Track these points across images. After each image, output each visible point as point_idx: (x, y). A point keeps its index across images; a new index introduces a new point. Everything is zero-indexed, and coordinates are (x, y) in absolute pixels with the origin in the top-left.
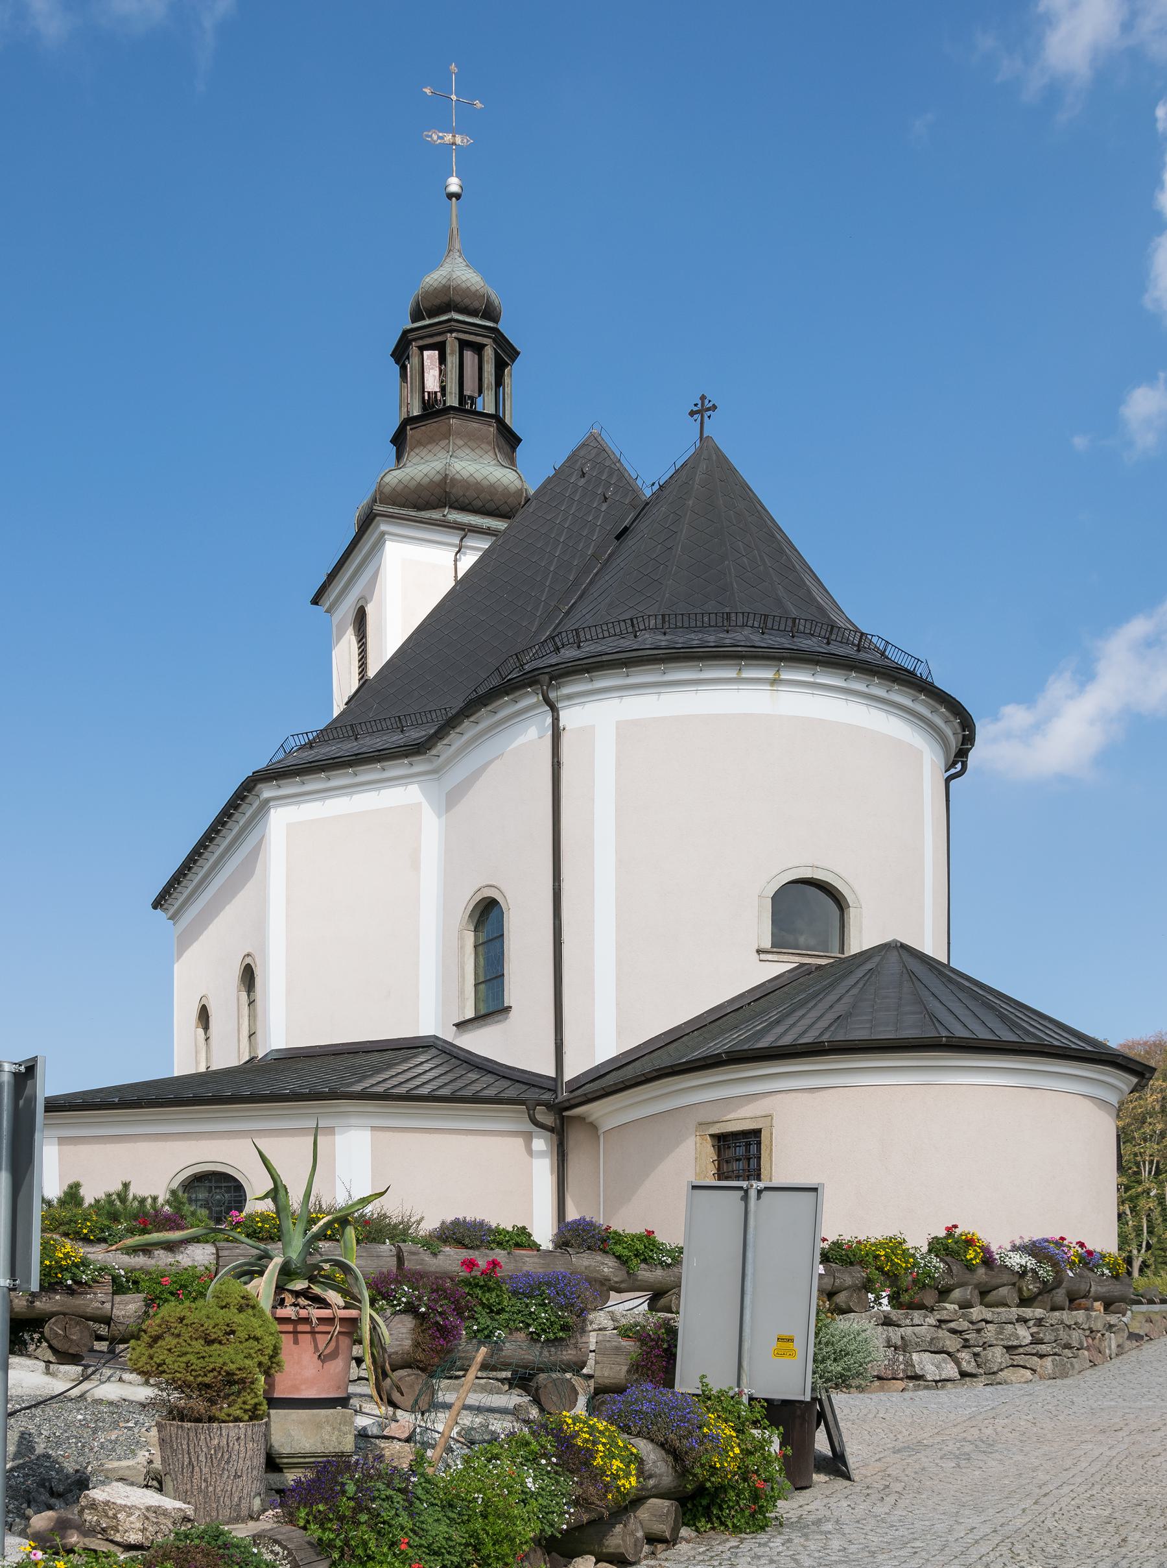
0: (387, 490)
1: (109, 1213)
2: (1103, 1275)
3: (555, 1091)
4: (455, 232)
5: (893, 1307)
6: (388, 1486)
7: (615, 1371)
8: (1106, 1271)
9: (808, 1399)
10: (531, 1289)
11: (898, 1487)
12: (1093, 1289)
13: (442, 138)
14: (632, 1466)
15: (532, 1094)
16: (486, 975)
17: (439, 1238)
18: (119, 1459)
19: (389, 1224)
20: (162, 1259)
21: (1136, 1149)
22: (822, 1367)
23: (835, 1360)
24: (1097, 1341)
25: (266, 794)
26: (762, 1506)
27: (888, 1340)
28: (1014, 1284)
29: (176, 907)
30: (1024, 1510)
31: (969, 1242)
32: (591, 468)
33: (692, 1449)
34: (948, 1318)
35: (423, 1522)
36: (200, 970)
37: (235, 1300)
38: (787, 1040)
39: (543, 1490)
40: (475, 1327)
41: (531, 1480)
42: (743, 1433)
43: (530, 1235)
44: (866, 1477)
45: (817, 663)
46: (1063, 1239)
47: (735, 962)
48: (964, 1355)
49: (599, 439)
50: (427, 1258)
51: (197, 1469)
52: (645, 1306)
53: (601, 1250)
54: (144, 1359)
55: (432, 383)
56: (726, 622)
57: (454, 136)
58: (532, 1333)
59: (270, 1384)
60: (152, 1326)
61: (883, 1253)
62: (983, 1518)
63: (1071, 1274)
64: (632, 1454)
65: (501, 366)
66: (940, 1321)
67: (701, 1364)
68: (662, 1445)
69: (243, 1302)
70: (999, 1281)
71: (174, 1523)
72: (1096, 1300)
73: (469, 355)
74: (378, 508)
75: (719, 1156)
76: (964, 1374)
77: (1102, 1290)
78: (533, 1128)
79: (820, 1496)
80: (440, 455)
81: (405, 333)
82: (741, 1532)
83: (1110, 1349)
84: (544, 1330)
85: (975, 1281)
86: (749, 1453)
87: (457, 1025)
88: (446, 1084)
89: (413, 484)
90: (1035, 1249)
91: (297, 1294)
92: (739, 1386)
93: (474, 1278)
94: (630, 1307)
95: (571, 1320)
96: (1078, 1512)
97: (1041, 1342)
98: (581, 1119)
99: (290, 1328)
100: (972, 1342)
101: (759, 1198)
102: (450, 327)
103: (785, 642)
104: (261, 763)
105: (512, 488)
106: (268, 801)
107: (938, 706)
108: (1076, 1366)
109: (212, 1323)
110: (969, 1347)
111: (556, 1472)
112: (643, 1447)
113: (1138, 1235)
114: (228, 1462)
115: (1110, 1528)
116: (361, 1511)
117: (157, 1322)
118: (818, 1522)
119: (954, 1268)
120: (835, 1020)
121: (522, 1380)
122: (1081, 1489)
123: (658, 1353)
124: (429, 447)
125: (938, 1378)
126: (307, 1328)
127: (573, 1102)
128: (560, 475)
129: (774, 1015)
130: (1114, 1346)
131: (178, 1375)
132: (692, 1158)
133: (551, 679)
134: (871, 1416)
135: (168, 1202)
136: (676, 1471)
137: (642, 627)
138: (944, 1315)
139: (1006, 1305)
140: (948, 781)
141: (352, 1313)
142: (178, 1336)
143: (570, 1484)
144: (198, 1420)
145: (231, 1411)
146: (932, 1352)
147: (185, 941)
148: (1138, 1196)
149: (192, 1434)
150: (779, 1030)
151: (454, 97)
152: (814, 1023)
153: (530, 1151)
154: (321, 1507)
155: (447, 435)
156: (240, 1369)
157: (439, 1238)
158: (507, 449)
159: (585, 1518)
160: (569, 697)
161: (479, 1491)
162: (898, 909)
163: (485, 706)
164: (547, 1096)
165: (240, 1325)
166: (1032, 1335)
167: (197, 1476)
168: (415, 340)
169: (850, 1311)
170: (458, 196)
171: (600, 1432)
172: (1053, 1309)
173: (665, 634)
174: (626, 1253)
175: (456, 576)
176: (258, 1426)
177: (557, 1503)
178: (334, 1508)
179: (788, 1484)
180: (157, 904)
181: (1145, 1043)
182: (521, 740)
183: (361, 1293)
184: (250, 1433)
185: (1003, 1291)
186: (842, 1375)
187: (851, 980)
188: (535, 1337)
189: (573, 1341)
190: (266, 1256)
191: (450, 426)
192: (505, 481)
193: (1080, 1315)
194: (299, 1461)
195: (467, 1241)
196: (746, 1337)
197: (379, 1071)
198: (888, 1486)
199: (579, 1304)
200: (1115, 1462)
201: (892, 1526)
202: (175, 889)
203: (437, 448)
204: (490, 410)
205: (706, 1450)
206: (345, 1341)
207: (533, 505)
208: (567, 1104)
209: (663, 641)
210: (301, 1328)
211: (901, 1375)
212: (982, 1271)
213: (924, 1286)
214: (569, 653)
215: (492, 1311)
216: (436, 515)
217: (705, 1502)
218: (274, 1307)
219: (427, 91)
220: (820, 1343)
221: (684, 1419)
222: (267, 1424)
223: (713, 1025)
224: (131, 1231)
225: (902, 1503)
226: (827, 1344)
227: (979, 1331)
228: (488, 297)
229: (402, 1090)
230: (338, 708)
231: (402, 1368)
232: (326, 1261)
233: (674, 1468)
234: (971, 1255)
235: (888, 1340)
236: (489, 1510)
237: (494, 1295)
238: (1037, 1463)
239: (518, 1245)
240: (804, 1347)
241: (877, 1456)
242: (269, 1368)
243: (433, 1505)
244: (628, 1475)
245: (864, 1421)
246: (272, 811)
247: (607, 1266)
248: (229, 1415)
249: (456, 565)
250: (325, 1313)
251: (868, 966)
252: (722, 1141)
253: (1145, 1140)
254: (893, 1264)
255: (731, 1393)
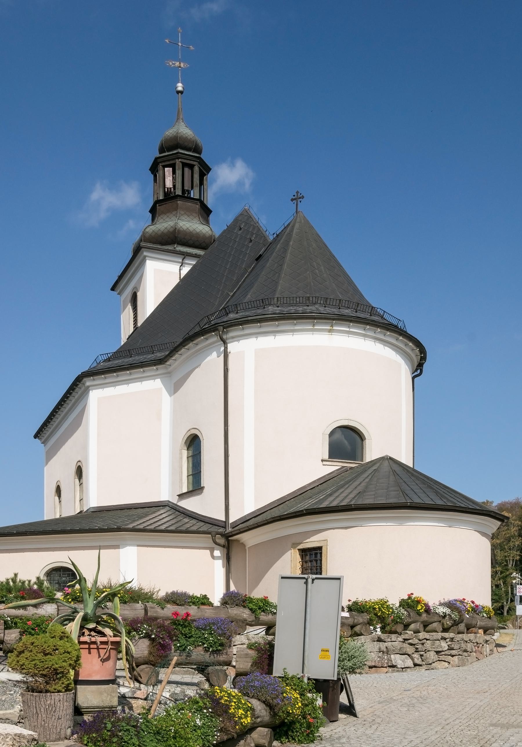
0: (147, 235)
1: (7, 588)
2: (483, 616)
3: (225, 527)
4: (180, 110)
5: (382, 632)
6: (128, 724)
7: (245, 665)
8: (485, 615)
9: (336, 679)
10: (208, 626)
11: (379, 720)
12: (478, 623)
13: (174, 64)
14: (249, 713)
15: (214, 529)
16: (192, 472)
17: (165, 600)
18: (6, 710)
19: (144, 593)
20: (31, 611)
21: (506, 554)
22: (342, 663)
23: (349, 660)
24: (480, 648)
25: (88, 384)
26: (312, 731)
27: (380, 649)
28: (440, 621)
29: (45, 437)
30: (436, 732)
31: (418, 602)
32: (244, 224)
33: (278, 704)
34: (408, 638)
35: (144, 742)
36: (58, 469)
37: (58, 634)
38: (334, 504)
39: (204, 724)
40: (178, 645)
41: (198, 720)
42: (304, 696)
43: (208, 599)
44: (364, 716)
45: (351, 321)
46: (464, 599)
47: (311, 466)
48: (416, 656)
49: (248, 211)
50: (159, 610)
51: (40, 715)
52: (264, 633)
53: (242, 606)
54: (14, 663)
55: (169, 183)
56: (308, 301)
57: (180, 63)
58: (205, 647)
59: (77, 674)
60: (20, 647)
61: (377, 607)
62: (417, 736)
63: (468, 616)
64: (249, 707)
65: (202, 176)
66: (404, 639)
67: (285, 663)
68: (264, 702)
69: (62, 635)
70: (433, 620)
71: (28, 742)
72: (480, 628)
73: (186, 170)
74: (143, 244)
75: (302, 559)
76: (416, 665)
77: (483, 624)
78: (214, 545)
79: (342, 725)
80: (172, 218)
81: (156, 159)
82: (302, 743)
83: (486, 652)
84: (211, 646)
85: (422, 620)
86: (307, 705)
87: (179, 496)
88: (173, 524)
89: (160, 232)
90: (450, 605)
91: (90, 630)
92: (303, 673)
93: (178, 621)
94: (256, 634)
95: (225, 641)
96: (462, 733)
97: (452, 649)
98: (237, 541)
99: (87, 646)
100: (419, 649)
101: (313, 583)
102: (177, 156)
103: (336, 311)
104: (86, 369)
105: (207, 235)
106: (88, 387)
107: (408, 342)
108: (469, 660)
109: (47, 645)
110: (418, 652)
111: (211, 716)
112: (256, 704)
113: (506, 595)
114: (55, 712)
115: (476, 741)
116: (114, 737)
117: (21, 644)
118: (339, 738)
119: (411, 614)
120: (358, 494)
121: (202, 669)
122: (465, 722)
123: (266, 656)
124: (168, 214)
125: (403, 667)
126: (95, 646)
127: (233, 533)
128: (230, 229)
129: (329, 492)
130: (488, 650)
131: (31, 670)
132: (290, 562)
133: (224, 328)
134: (369, 685)
135: (35, 583)
136: (271, 714)
137: (267, 304)
138: (406, 636)
139: (436, 631)
140: (413, 378)
141: (117, 639)
142: (31, 651)
143: (218, 722)
144: (41, 692)
145: (56, 687)
146: (400, 654)
147: (50, 455)
148: (507, 576)
149: (37, 699)
150: (331, 498)
151: (180, 44)
152: (347, 496)
153: (213, 557)
154: (94, 735)
155: (176, 209)
156: (60, 667)
157: (165, 600)
158: (205, 215)
159: (225, 738)
160: (233, 338)
161: (173, 726)
162: (390, 439)
163: (192, 341)
164: (221, 530)
165: (60, 646)
166: (448, 646)
167: (40, 718)
168: (161, 162)
169: (361, 634)
170: (181, 92)
171: (233, 696)
172: (459, 633)
173: (278, 307)
174: (254, 607)
175: (180, 277)
176: (71, 695)
177: (211, 731)
178: (101, 736)
179: (325, 719)
180: (36, 436)
181: (511, 503)
182: (209, 358)
183: (122, 630)
184: (65, 698)
185: (435, 625)
186: (352, 667)
187: (365, 475)
188: (207, 649)
189: (225, 651)
190: (75, 611)
191: (177, 204)
192: (204, 231)
193: (471, 636)
194: (90, 710)
195: (178, 602)
196: (307, 649)
197: (141, 518)
198: (374, 720)
199: (228, 633)
200: (482, 708)
201: (374, 740)
202: (45, 429)
203: (166, 216)
204: (197, 197)
205: (285, 704)
206: (113, 653)
207: (217, 243)
208: (231, 534)
209: (277, 310)
210: (92, 646)
211: (386, 665)
212: (424, 615)
213: (397, 622)
214: (232, 316)
215: (186, 637)
216: (170, 248)
217: (285, 729)
218: (79, 636)
219: (167, 41)
220: (342, 652)
221: (274, 689)
222: (75, 694)
223: (301, 496)
224: (16, 598)
225: (380, 729)
226: (345, 652)
227: (423, 644)
228: (196, 142)
229: (152, 527)
230: (124, 340)
231: (144, 664)
232: (104, 614)
233: (270, 713)
234: (419, 607)
235: (380, 649)
236: (177, 735)
237: (187, 629)
238: (445, 708)
239: (203, 604)
240: (334, 655)
241: (371, 706)
242: (75, 666)
243: (150, 733)
244: (246, 717)
245: (363, 688)
246: (91, 391)
247: (245, 614)
248: (55, 689)
249: (180, 272)
250: (104, 639)
251: (375, 468)
252: (304, 552)
253: (510, 549)
254: (382, 612)
255: (298, 676)
